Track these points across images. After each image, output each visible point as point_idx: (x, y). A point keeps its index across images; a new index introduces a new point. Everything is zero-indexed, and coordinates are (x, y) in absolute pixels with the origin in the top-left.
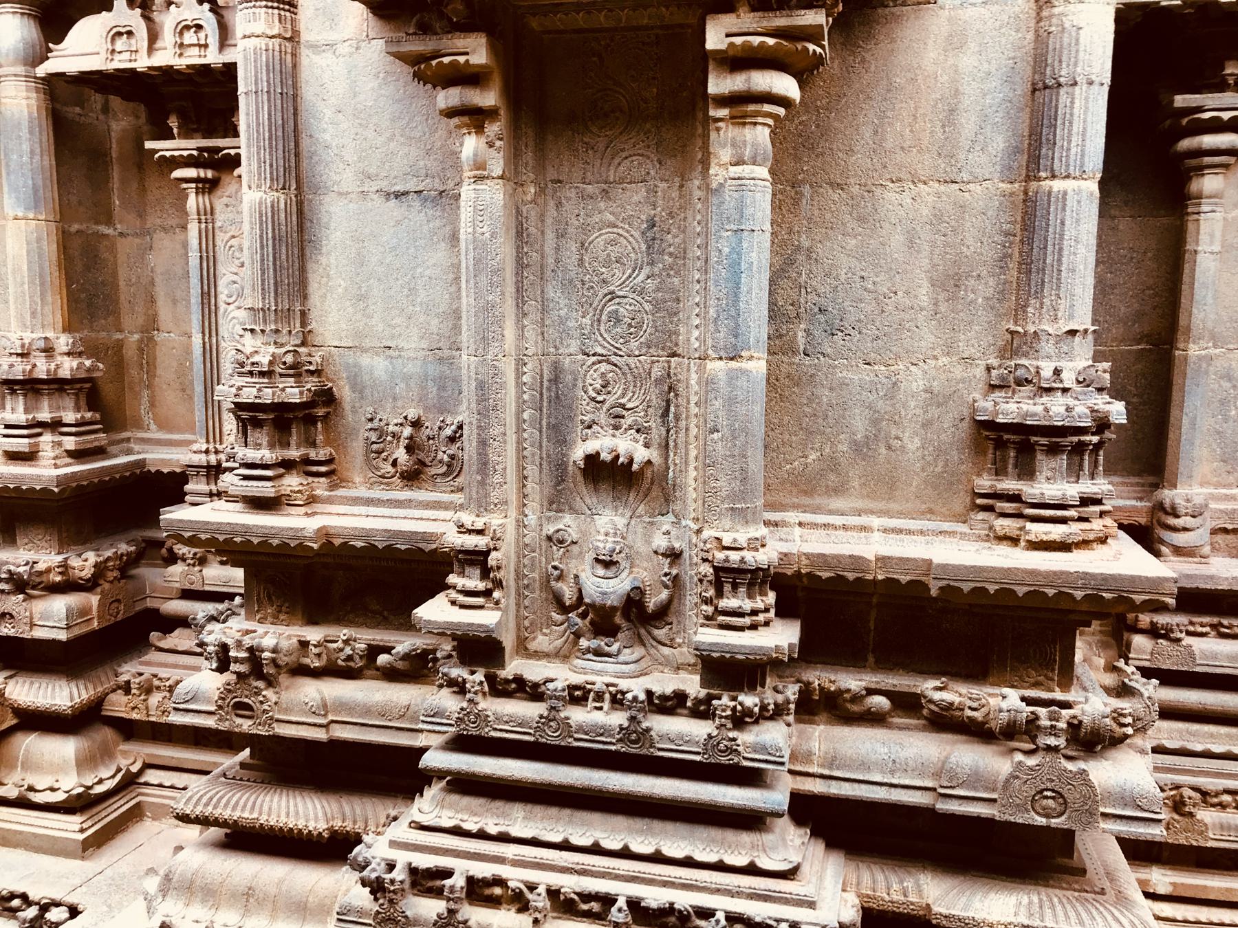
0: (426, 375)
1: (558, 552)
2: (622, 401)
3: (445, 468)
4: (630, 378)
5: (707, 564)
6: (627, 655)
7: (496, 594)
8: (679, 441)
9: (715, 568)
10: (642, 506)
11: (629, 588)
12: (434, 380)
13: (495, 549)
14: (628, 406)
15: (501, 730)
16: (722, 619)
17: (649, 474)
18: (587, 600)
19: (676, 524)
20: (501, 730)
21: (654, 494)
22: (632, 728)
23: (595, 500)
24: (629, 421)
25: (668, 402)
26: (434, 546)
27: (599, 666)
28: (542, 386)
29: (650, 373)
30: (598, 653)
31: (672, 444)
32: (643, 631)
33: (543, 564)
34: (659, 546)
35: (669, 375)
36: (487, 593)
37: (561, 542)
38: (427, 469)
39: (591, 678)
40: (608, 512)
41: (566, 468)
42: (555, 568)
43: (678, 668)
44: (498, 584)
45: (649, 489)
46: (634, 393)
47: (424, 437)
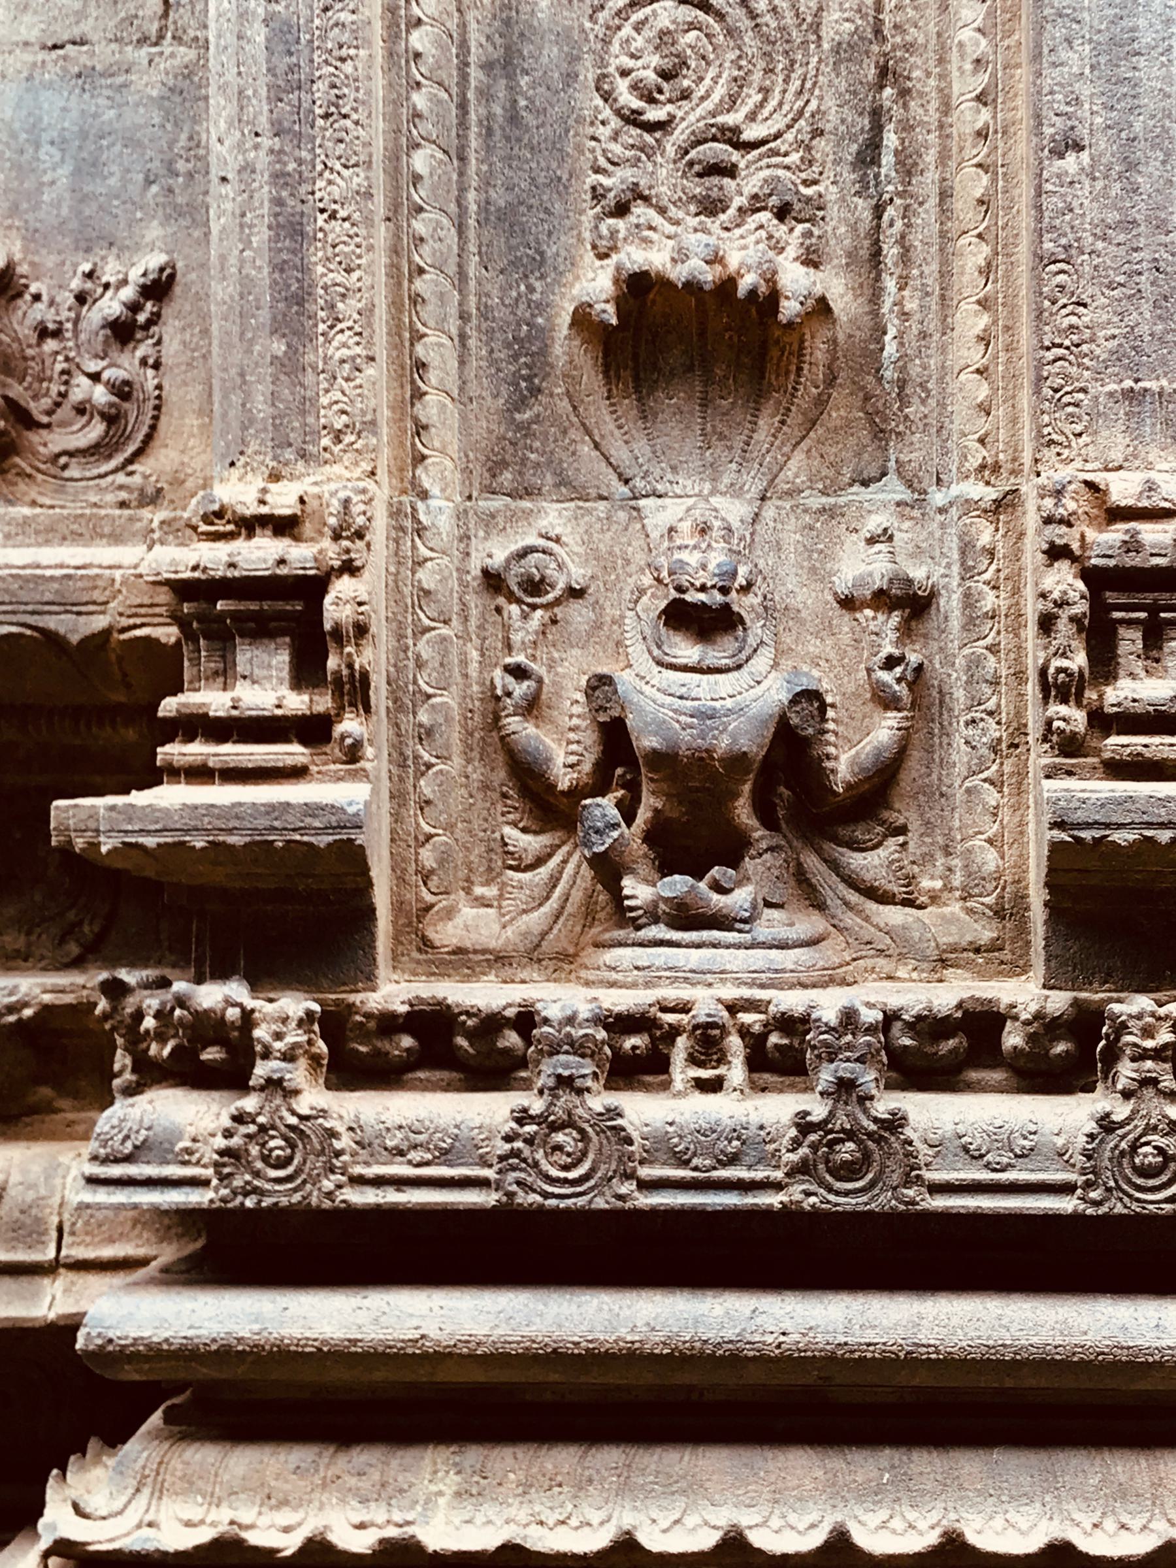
0: (35, 128)
1: (524, 624)
2: (730, 119)
3: (97, 430)
4: (751, 43)
5: (1064, 565)
6: (771, 925)
7: (350, 725)
8: (915, 239)
9: (1090, 576)
10: (798, 457)
11: (785, 697)
12: (61, 143)
13: (350, 568)
14: (751, 133)
15: (379, 1182)
16: (1117, 743)
17: (818, 352)
18: (646, 742)
19: (915, 505)
20: (379, 1182)
21: (835, 415)
22: (842, 1121)
23: (641, 447)
24: (751, 182)
25: (877, 116)
26: (99, 622)
27: (695, 958)
28: (464, 77)
29: (816, 28)
30: (687, 917)
31: (891, 252)
32: (811, 861)
33: (473, 669)
34: (859, 582)
35: (878, 32)
36: (313, 730)
37: (535, 586)
38: (34, 437)
39: (672, 993)
40: (686, 483)
41: (544, 351)
42: (519, 673)
43: (943, 962)
44: (355, 691)
45: (821, 402)
46: (766, 91)
47: (26, 332)
